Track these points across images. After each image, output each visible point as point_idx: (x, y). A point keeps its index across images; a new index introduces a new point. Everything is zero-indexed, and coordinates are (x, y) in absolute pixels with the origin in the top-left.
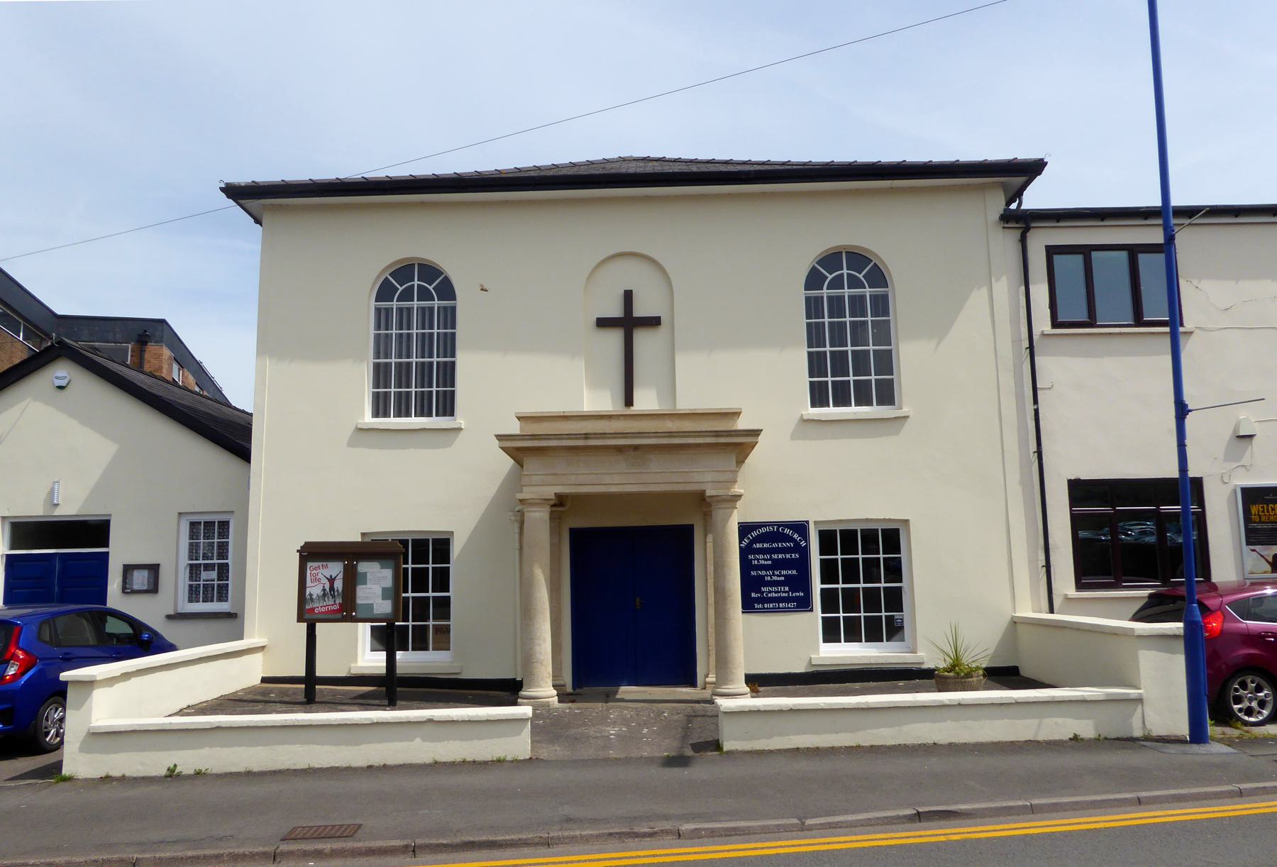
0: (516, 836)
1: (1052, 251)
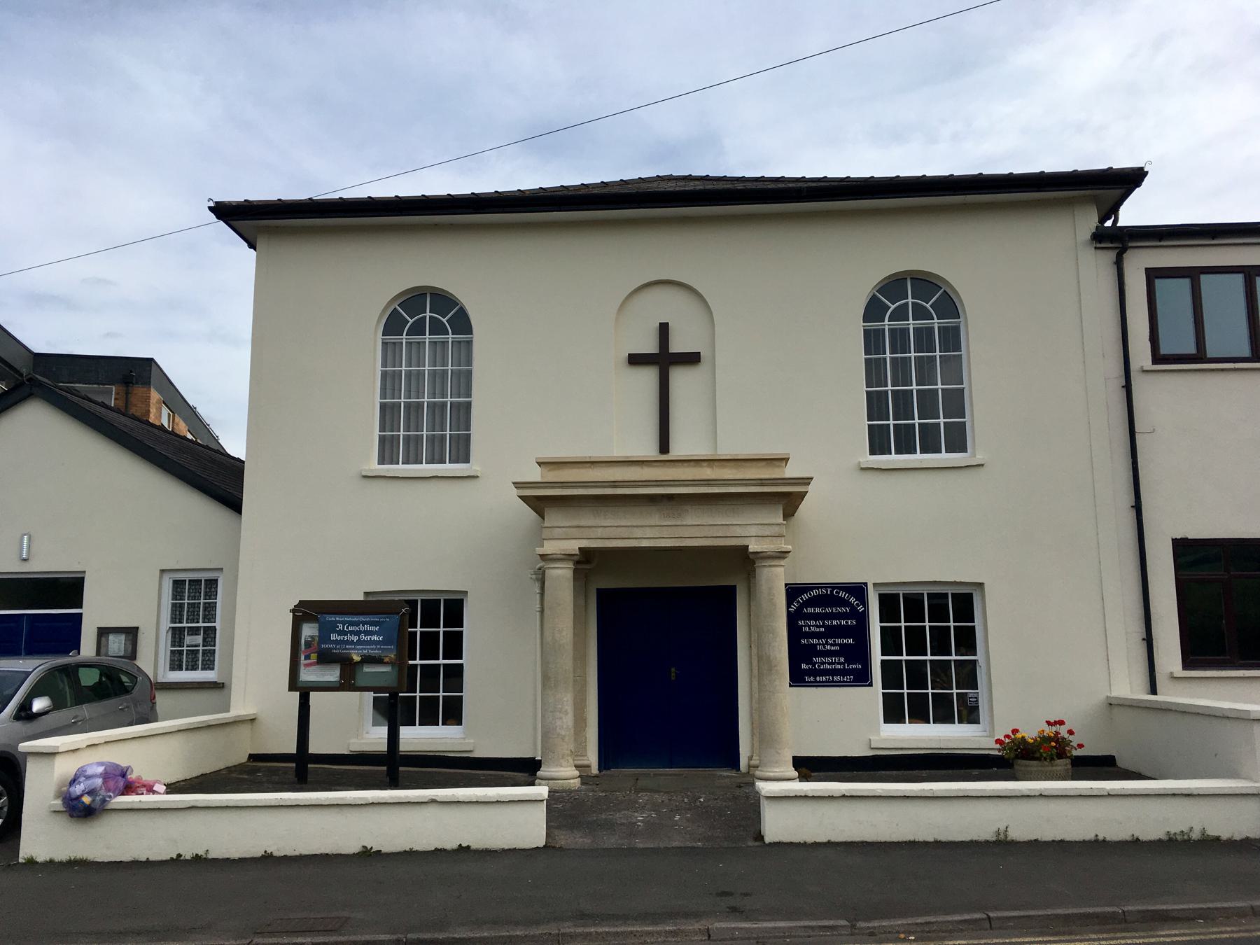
0: (522, 933)
1: (1153, 275)
